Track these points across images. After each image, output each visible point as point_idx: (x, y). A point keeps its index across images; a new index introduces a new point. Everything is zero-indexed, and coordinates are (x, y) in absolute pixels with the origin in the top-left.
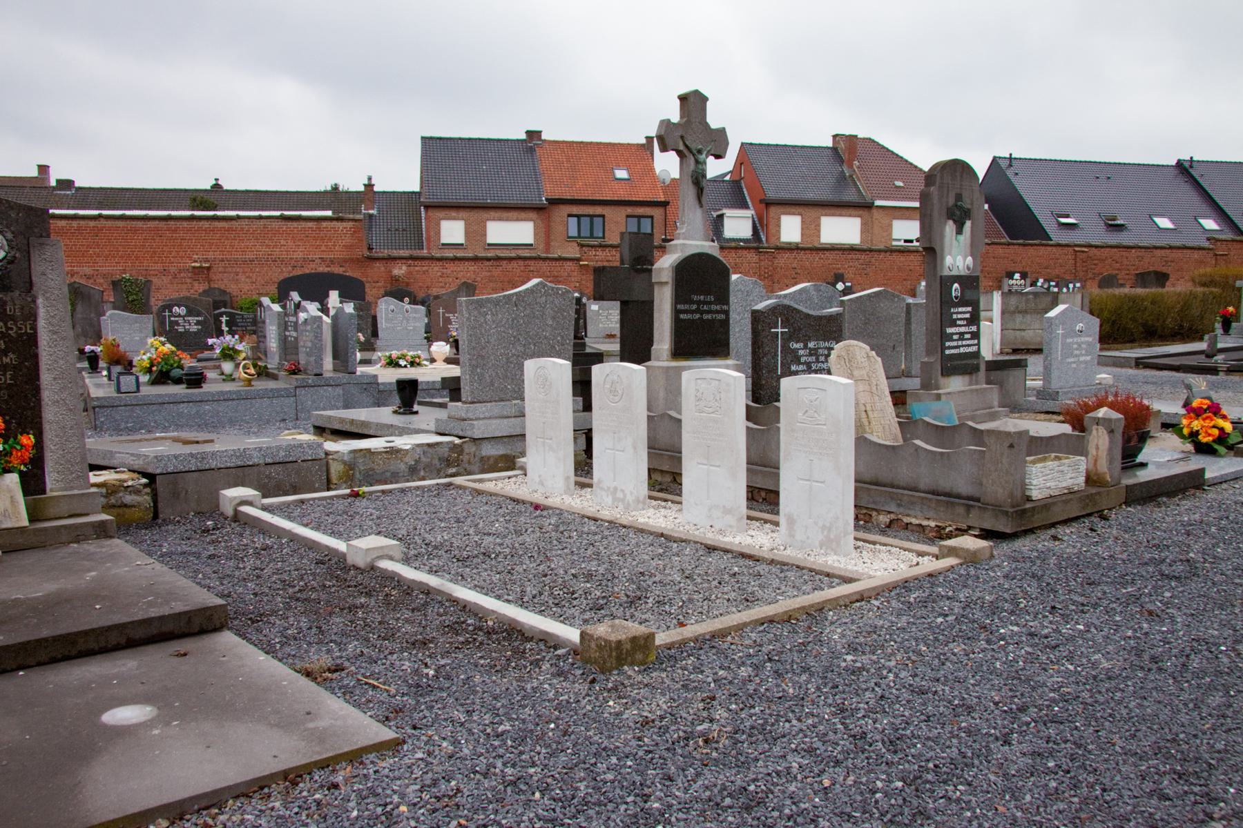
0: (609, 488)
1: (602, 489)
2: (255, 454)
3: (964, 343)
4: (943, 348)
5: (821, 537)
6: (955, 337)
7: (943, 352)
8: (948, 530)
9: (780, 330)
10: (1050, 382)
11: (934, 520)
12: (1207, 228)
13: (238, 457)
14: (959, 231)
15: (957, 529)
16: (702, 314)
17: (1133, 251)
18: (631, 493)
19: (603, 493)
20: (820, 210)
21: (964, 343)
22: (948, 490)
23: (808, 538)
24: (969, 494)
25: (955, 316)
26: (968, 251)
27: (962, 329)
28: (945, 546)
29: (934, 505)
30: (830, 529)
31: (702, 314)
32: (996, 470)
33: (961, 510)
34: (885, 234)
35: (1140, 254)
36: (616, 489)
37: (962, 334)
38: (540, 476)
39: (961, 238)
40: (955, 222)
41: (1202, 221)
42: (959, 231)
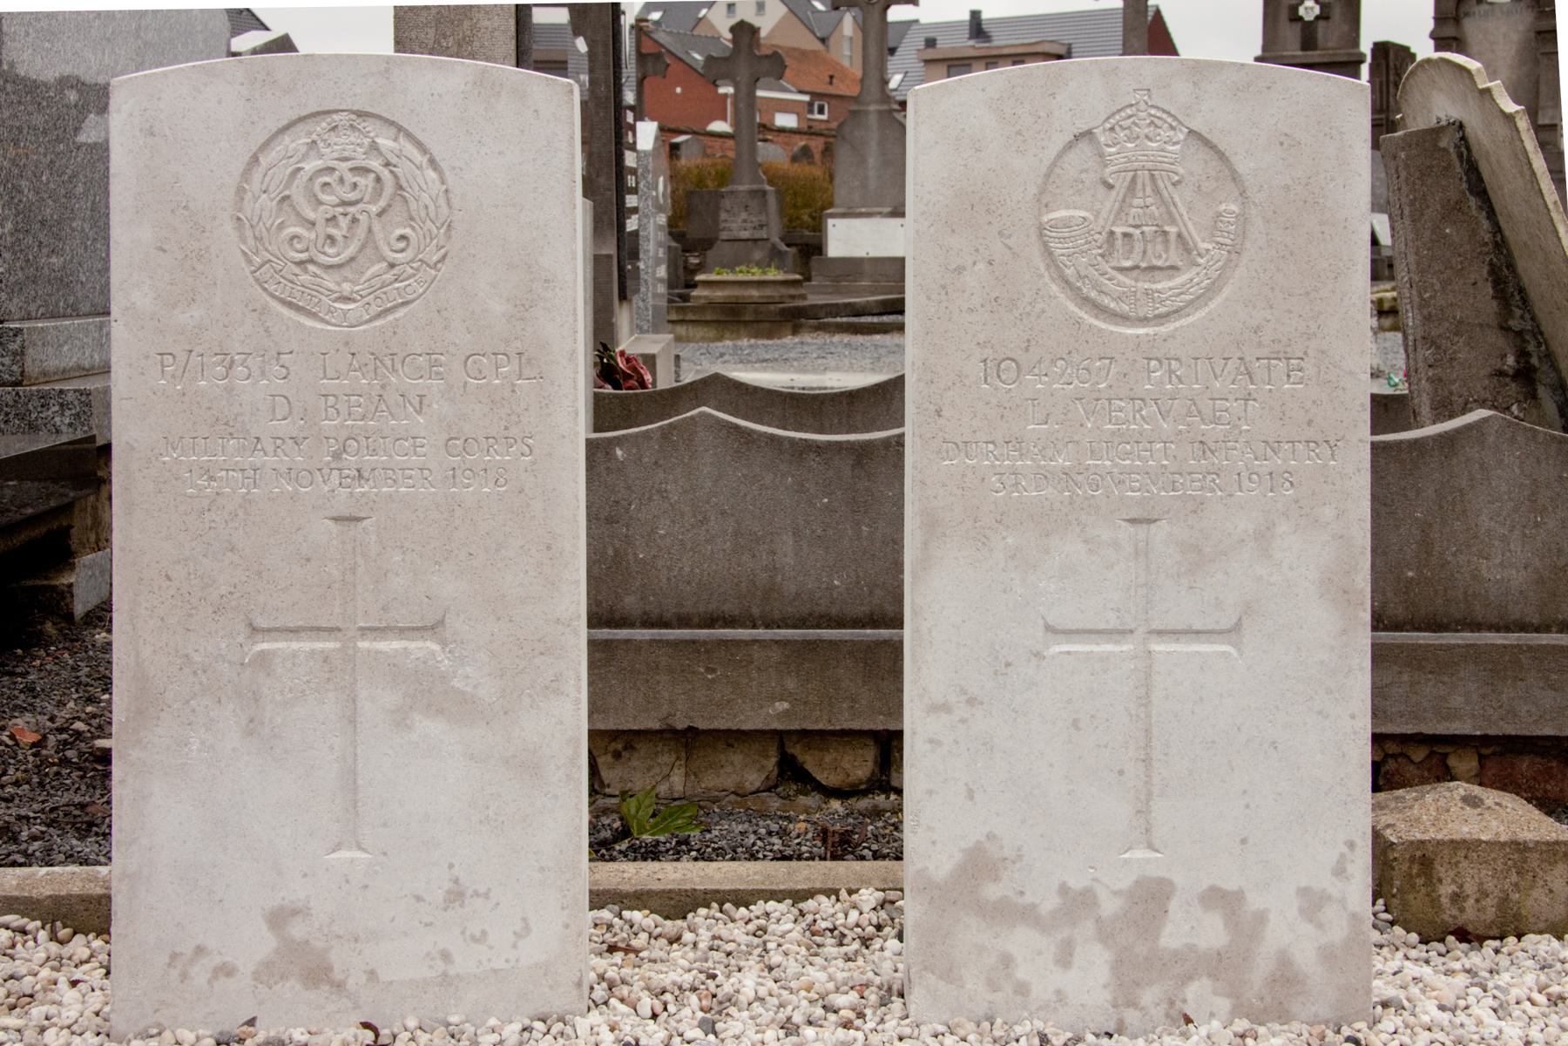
0: (1078, 902)
7: (621, 226)
19: (1022, 942)
38: (278, 919)
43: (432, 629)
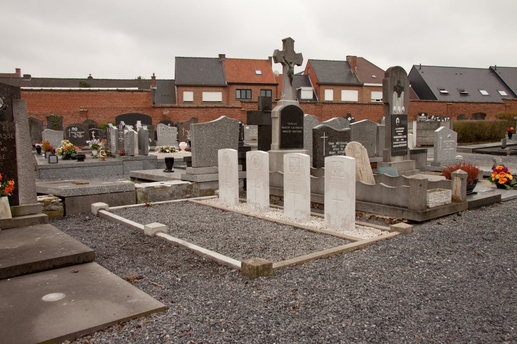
0: (253, 203)
1: (250, 203)
2: (106, 189)
3: (401, 142)
4: (392, 145)
5: (341, 223)
6: (397, 140)
8: (394, 220)
9: (324, 137)
10: (437, 159)
11: (389, 216)
12: (502, 94)
13: (99, 190)
14: (399, 96)
15: (398, 220)
16: (292, 131)
17: (471, 104)
18: (263, 205)
20: (341, 87)
21: (401, 142)
22: (394, 203)
23: (336, 223)
24: (403, 205)
25: (397, 131)
26: (403, 104)
27: (400, 137)
28: (393, 227)
29: (388, 210)
30: (345, 220)
31: (292, 131)
32: (414, 195)
33: (400, 212)
34: (368, 97)
35: (474, 106)
36: (256, 203)
37: (400, 139)
39: (400, 99)
40: (397, 92)
41: (500, 92)
42: (399, 96)
43: (229, 182)
